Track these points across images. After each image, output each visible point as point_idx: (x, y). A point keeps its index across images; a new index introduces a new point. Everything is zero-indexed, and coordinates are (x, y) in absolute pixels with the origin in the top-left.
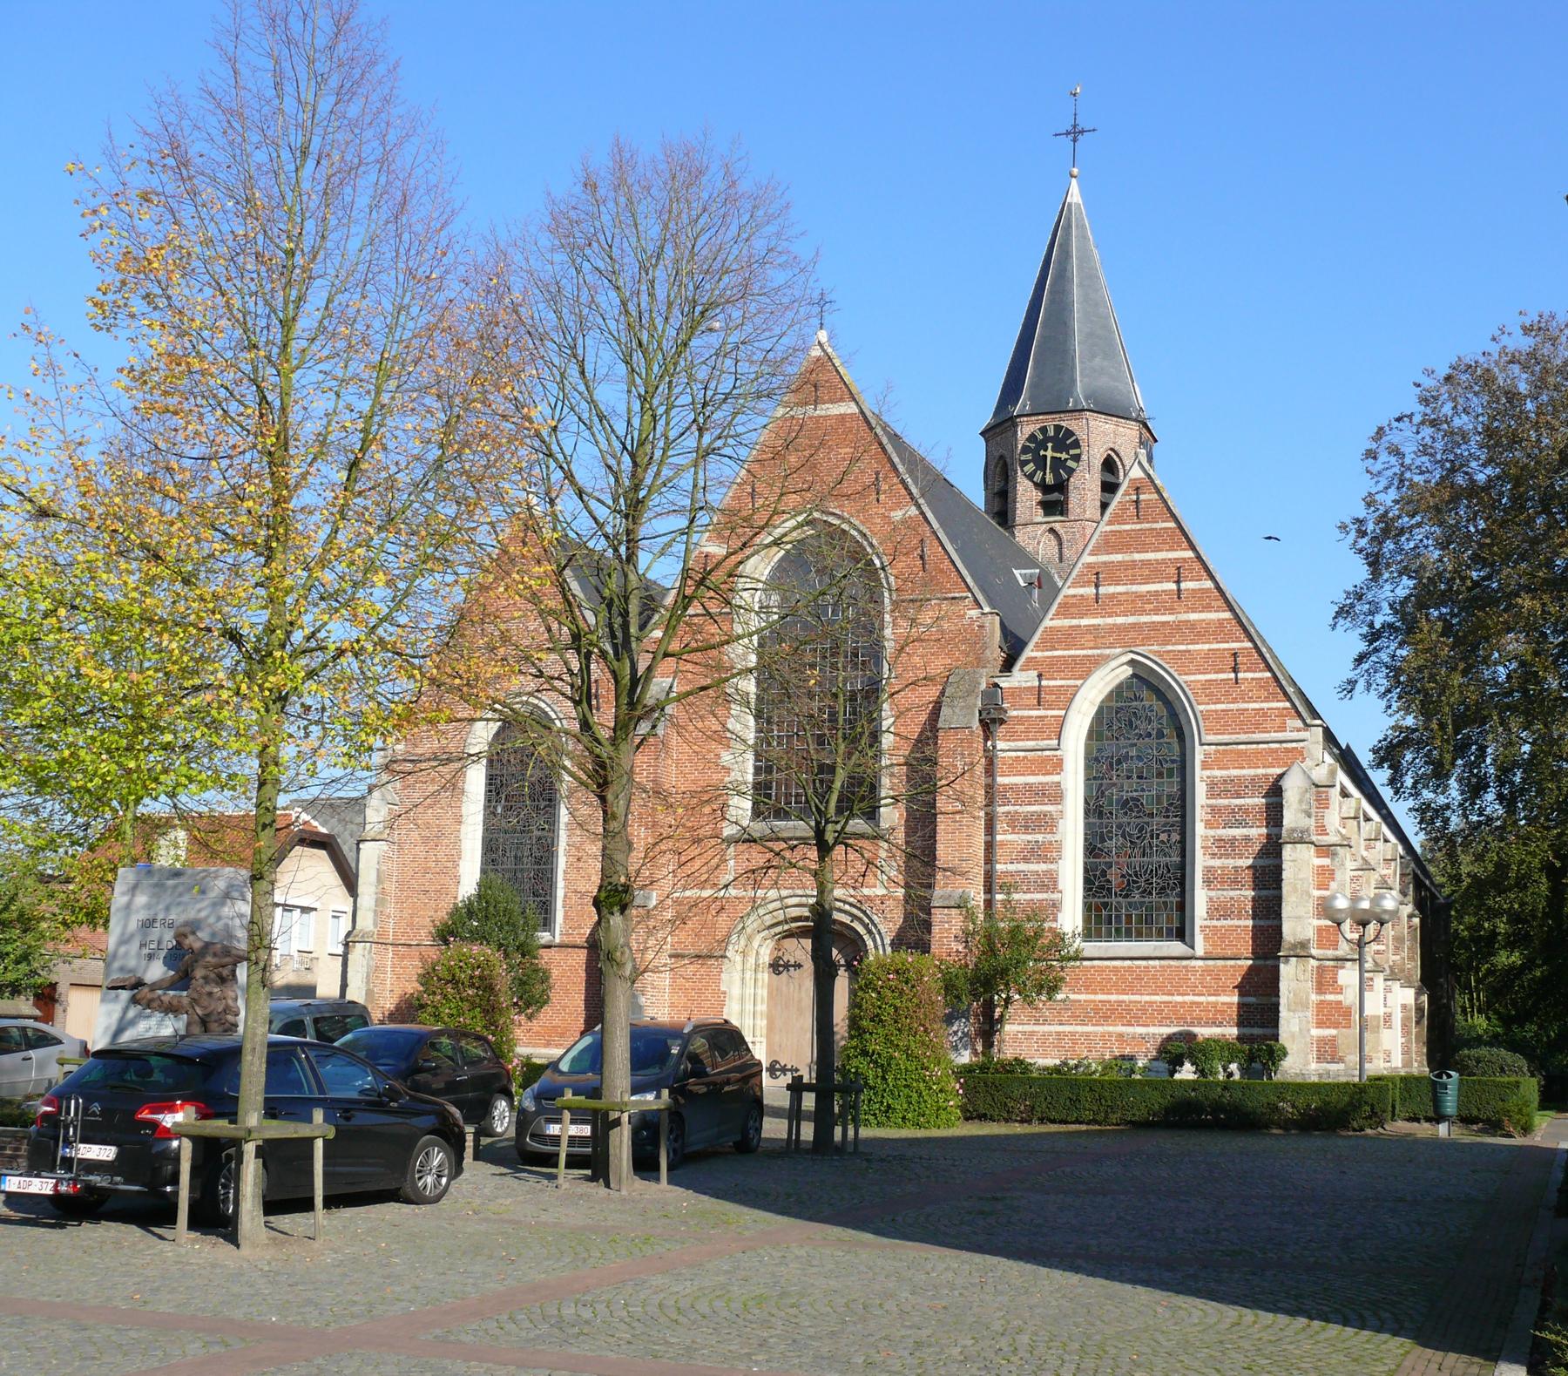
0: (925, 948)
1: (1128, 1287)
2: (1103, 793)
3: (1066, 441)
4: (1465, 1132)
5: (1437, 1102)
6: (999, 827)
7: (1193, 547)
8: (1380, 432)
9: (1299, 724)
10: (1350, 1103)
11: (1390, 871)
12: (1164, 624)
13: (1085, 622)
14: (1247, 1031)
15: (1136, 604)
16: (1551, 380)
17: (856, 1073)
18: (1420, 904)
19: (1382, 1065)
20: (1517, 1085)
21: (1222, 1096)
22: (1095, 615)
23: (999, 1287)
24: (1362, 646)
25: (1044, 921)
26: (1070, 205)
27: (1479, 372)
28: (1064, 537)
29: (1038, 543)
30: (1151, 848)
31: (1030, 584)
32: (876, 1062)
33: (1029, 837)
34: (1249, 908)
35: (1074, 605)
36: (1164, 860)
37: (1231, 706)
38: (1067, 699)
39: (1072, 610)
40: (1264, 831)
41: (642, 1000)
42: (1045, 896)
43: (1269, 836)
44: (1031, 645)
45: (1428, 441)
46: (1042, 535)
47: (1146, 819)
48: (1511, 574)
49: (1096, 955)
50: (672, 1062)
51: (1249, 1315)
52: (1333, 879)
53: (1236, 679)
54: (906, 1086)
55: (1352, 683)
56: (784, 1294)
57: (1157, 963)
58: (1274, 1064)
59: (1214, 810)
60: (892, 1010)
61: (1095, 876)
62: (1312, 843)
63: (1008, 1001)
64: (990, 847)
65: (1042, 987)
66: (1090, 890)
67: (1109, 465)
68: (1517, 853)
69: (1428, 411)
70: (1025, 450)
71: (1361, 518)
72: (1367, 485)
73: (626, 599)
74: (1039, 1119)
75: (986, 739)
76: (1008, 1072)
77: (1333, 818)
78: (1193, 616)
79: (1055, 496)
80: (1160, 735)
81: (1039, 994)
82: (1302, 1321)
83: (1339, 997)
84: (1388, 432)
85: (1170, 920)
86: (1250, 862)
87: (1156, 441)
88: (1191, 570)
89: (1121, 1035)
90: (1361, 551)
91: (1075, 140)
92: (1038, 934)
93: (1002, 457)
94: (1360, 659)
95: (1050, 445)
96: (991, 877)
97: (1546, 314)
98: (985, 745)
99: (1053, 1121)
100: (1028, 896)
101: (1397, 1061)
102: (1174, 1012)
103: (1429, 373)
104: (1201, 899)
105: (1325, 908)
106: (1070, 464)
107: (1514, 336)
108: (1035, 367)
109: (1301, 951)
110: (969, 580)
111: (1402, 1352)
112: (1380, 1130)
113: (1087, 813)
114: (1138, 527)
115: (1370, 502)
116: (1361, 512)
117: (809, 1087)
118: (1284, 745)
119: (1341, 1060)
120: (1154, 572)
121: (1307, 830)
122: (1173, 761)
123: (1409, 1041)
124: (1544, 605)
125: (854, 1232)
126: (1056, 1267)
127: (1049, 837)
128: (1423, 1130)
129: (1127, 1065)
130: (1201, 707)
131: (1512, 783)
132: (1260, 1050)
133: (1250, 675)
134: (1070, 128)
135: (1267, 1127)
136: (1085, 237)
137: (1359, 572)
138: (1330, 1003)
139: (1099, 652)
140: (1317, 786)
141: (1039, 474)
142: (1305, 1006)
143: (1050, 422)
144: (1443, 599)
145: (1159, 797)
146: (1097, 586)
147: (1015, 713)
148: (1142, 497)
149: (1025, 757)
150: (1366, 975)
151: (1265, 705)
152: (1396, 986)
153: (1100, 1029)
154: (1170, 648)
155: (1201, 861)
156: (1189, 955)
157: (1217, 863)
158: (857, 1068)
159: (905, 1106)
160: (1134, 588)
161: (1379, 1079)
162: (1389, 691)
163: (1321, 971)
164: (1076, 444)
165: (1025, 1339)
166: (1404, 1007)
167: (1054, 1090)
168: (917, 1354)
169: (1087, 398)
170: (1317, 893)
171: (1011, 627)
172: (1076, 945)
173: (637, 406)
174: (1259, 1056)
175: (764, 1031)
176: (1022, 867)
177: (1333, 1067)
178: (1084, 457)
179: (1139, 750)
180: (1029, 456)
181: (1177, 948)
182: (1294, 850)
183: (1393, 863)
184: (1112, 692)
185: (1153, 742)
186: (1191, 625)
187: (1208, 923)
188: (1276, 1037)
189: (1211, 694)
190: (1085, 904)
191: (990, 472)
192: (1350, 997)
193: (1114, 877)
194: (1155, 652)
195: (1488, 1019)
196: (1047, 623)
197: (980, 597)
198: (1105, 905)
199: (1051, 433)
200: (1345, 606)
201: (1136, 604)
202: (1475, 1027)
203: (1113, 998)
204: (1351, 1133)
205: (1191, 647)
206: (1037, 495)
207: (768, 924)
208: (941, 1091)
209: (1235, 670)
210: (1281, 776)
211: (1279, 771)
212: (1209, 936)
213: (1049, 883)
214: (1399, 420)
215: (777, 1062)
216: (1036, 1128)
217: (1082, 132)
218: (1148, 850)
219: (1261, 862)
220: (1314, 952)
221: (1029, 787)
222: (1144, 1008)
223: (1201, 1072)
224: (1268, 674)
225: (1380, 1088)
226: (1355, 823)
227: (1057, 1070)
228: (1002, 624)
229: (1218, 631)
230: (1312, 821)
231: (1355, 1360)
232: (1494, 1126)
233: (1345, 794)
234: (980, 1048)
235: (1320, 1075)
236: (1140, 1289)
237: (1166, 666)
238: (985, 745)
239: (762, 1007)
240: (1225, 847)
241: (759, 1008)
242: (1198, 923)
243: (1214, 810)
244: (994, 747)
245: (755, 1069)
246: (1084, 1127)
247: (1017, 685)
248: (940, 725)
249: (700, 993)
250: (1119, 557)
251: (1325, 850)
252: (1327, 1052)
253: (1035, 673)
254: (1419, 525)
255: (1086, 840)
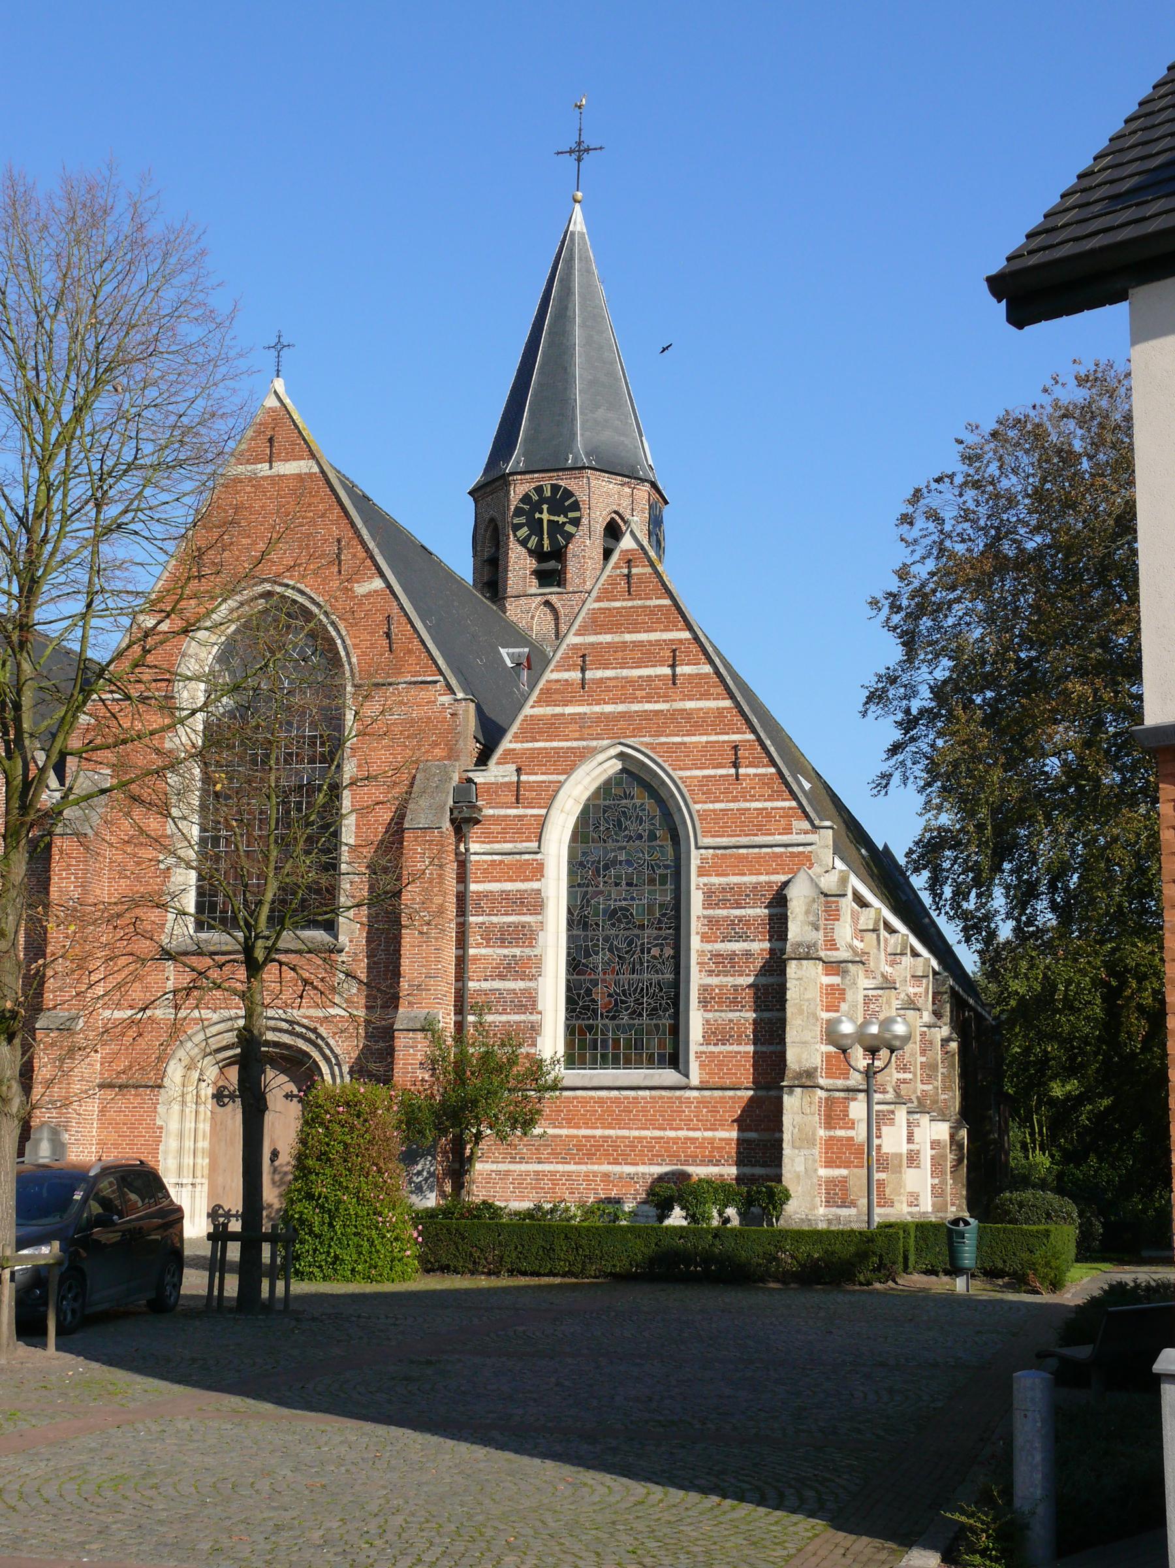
0: (386, 1079)
1: (537, 1461)
2: (588, 901)
3: (563, 502)
4: (988, 1287)
5: (953, 1254)
6: (472, 939)
7: (689, 627)
8: (917, 495)
9: (806, 825)
10: (857, 1254)
11: (921, 990)
12: (657, 713)
13: (569, 710)
14: (748, 1170)
15: (627, 690)
16: (1109, 437)
17: (300, 1219)
18: (961, 1027)
19: (905, 1209)
20: (1047, 1233)
21: (713, 1245)
22: (581, 702)
23: (393, 1462)
24: (897, 735)
25: (520, 1045)
26: (573, 234)
27: (1029, 427)
28: (562, 611)
29: (533, 618)
30: (642, 964)
31: (518, 664)
32: (322, 1207)
33: (505, 951)
34: (750, 1032)
35: (557, 691)
36: (655, 977)
37: (732, 805)
38: (548, 796)
39: (555, 697)
40: (767, 945)
41: (66, 1137)
42: (522, 1017)
43: (772, 951)
44: (509, 736)
45: (971, 505)
46: (536, 608)
47: (636, 932)
48: (1062, 657)
49: (579, 1084)
50: (74, 1209)
51: (657, 1492)
52: (844, 1000)
53: (737, 774)
54: (355, 1234)
55: (887, 777)
56: (149, 1474)
57: (647, 1093)
58: (775, 1208)
59: (712, 922)
60: (341, 1148)
61: (579, 995)
62: (820, 959)
63: (478, 1137)
64: (461, 962)
65: (516, 1121)
66: (573, 1011)
67: (613, 531)
68: (1064, 972)
69: (971, 471)
70: (519, 512)
71: (895, 590)
72: (901, 555)
73: (19, 693)
74: (508, 1271)
75: (459, 841)
76: (475, 1217)
77: (844, 932)
78: (690, 705)
79: (552, 565)
80: (652, 837)
81: (514, 1128)
82: (715, 1499)
83: (851, 1133)
84: (926, 494)
85: (661, 1044)
86: (751, 980)
87: (666, 503)
88: (688, 653)
89: (606, 1175)
90: (895, 628)
91: (579, 160)
92: (512, 1061)
93: (492, 520)
94: (895, 749)
95: (545, 507)
96: (462, 997)
97: (1103, 362)
98: (457, 847)
99: (524, 1274)
100: (504, 1018)
101: (927, 1205)
102: (664, 1150)
103: (973, 428)
104: (696, 1022)
105: (831, 1035)
106: (569, 528)
107: (1068, 387)
108: (530, 420)
109: (807, 1081)
110: (441, 661)
111: (811, 1535)
112: (890, 1283)
113: (570, 923)
114: (630, 604)
115: (903, 574)
116: (894, 585)
117: (234, 1237)
118: (790, 849)
119: (853, 1204)
120: (646, 654)
121: (815, 945)
122: (666, 867)
123: (943, 1182)
124: (1096, 691)
125: (252, 1402)
126: (466, 1440)
127: (528, 951)
128: (940, 1284)
129: (610, 1209)
130: (698, 807)
131: (1066, 889)
132: (759, 1192)
133: (752, 771)
134: (574, 146)
135: (762, 1280)
136: (589, 271)
137: (892, 652)
138: (840, 1139)
139: (584, 743)
140: (826, 895)
141: (534, 540)
142: (810, 1142)
143: (547, 481)
144: (989, 681)
145: (650, 907)
146: (583, 670)
147: (491, 812)
148: (634, 571)
149: (501, 862)
150: (876, 1107)
151: (769, 805)
152: (924, 1119)
153: (583, 1168)
154: (663, 739)
155: (697, 979)
156: (683, 1084)
157: (714, 981)
158: (301, 1213)
159: (355, 1257)
160: (625, 672)
161: (890, 1226)
162: (929, 784)
163: (830, 1103)
164: (576, 506)
165: (399, 1520)
166: (935, 1144)
167: (525, 1237)
168: (273, 1539)
169: (588, 455)
170: (826, 1015)
171: (490, 713)
172: (553, 1074)
173: (34, 472)
174: (758, 1200)
175: (206, 1172)
176: (497, 984)
177: (844, 1212)
178: (584, 521)
179: (628, 854)
180: (523, 520)
181: (669, 1076)
182: (800, 967)
183: (924, 981)
184: (599, 788)
185: (643, 844)
186: (687, 714)
187: (704, 1048)
188: (778, 1178)
189: (709, 792)
190: (567, 1027)
191: (479, 537)
192: (859, 1134)
193: (600, 996)
194: (647, 745)
195: (1052, 1156)
196: (527, 711)
197: (453, 682)
198: (590, 1028)
199: (548, 493)
200: (877, 690)
201: (627, 690)
202: (1036, 1165)
203: (598, 1132)
204: (857, 1288)
205: (687, 739)
206: (531, 563)
207: (214, 1047)
208: (396, 1239)
209: (736, 765)
210: (786, 884)
211: (784, 878)
212: (708, 1060)
213: (528, 1002)
214: (938, 480)
215: (220, 1207)
216: (504, 1281)
217: (587, 150)
218: (637, 967)
219: (763, 980)
220: (822, 1082)
221: (505, 896)
222: (633, 1144)
223: (692, 1217)
224: (773, 770)
225: (889, 1237)
226: (874, 936)
227: (529, 1214)
228: (479, 711)
229: (716, 722)
230: (820, 936)
231: (754, 1544)
232: (1019, 1281)
233: (862, 903)
234: (448, 1189)
235: (829, 1221)
236: (549, 1464)
237: (660, 760)
238: (457, 847)
239: (204, 1144)
240: (723, 963)
241: (200, 1144)
242: (694, 1048)
243: (712, 922)
244: (467, 850)
245: (176, 1216)
246: (558, 1280)
247: (493, 780)
248: (406, 825)
249: (132, 1128)
250: (607, 638)
251: (835, 967)
252: (837, 1193)
253: (514, 767)
254: (958, 600)
255: (569, 954)
